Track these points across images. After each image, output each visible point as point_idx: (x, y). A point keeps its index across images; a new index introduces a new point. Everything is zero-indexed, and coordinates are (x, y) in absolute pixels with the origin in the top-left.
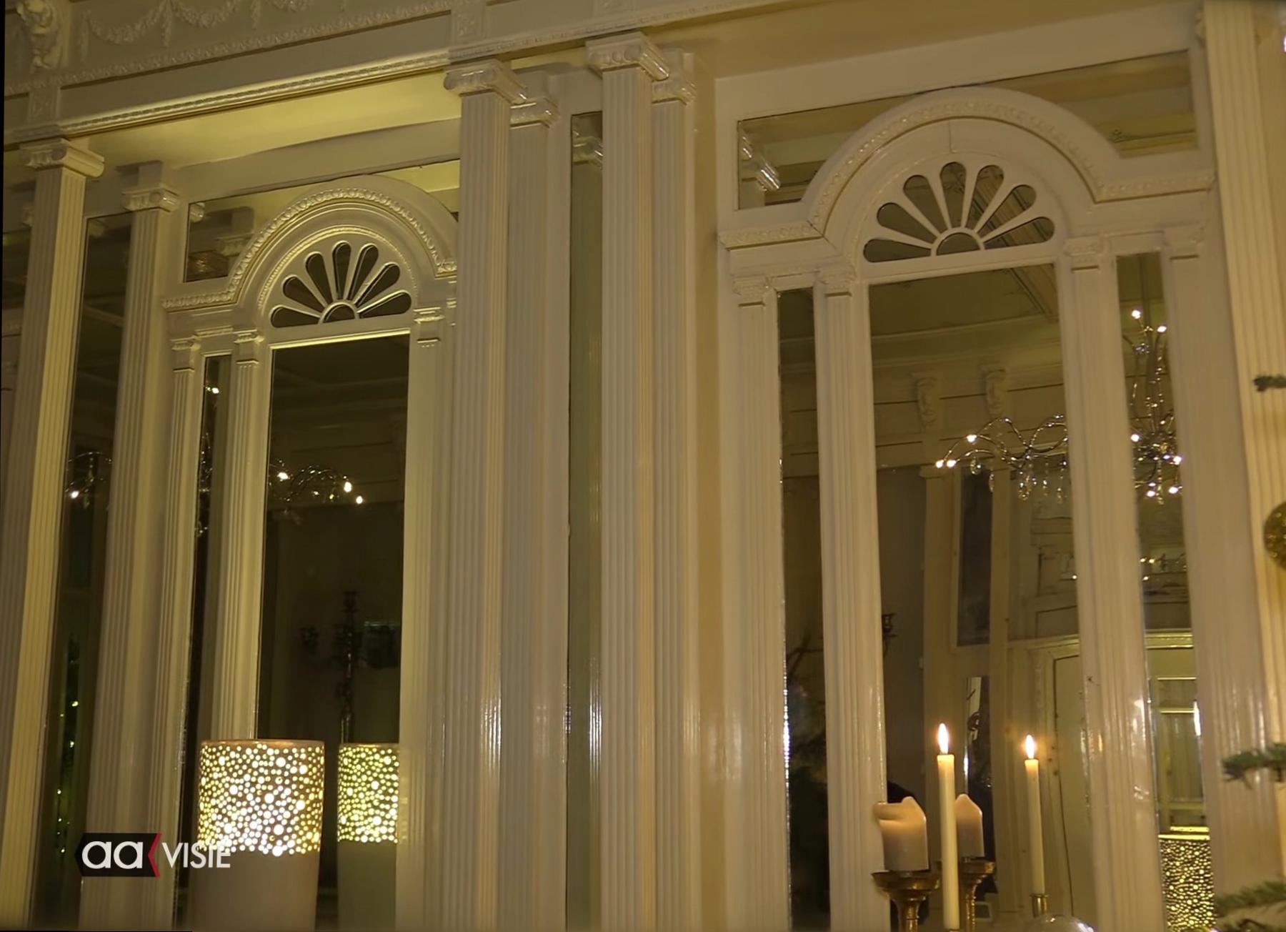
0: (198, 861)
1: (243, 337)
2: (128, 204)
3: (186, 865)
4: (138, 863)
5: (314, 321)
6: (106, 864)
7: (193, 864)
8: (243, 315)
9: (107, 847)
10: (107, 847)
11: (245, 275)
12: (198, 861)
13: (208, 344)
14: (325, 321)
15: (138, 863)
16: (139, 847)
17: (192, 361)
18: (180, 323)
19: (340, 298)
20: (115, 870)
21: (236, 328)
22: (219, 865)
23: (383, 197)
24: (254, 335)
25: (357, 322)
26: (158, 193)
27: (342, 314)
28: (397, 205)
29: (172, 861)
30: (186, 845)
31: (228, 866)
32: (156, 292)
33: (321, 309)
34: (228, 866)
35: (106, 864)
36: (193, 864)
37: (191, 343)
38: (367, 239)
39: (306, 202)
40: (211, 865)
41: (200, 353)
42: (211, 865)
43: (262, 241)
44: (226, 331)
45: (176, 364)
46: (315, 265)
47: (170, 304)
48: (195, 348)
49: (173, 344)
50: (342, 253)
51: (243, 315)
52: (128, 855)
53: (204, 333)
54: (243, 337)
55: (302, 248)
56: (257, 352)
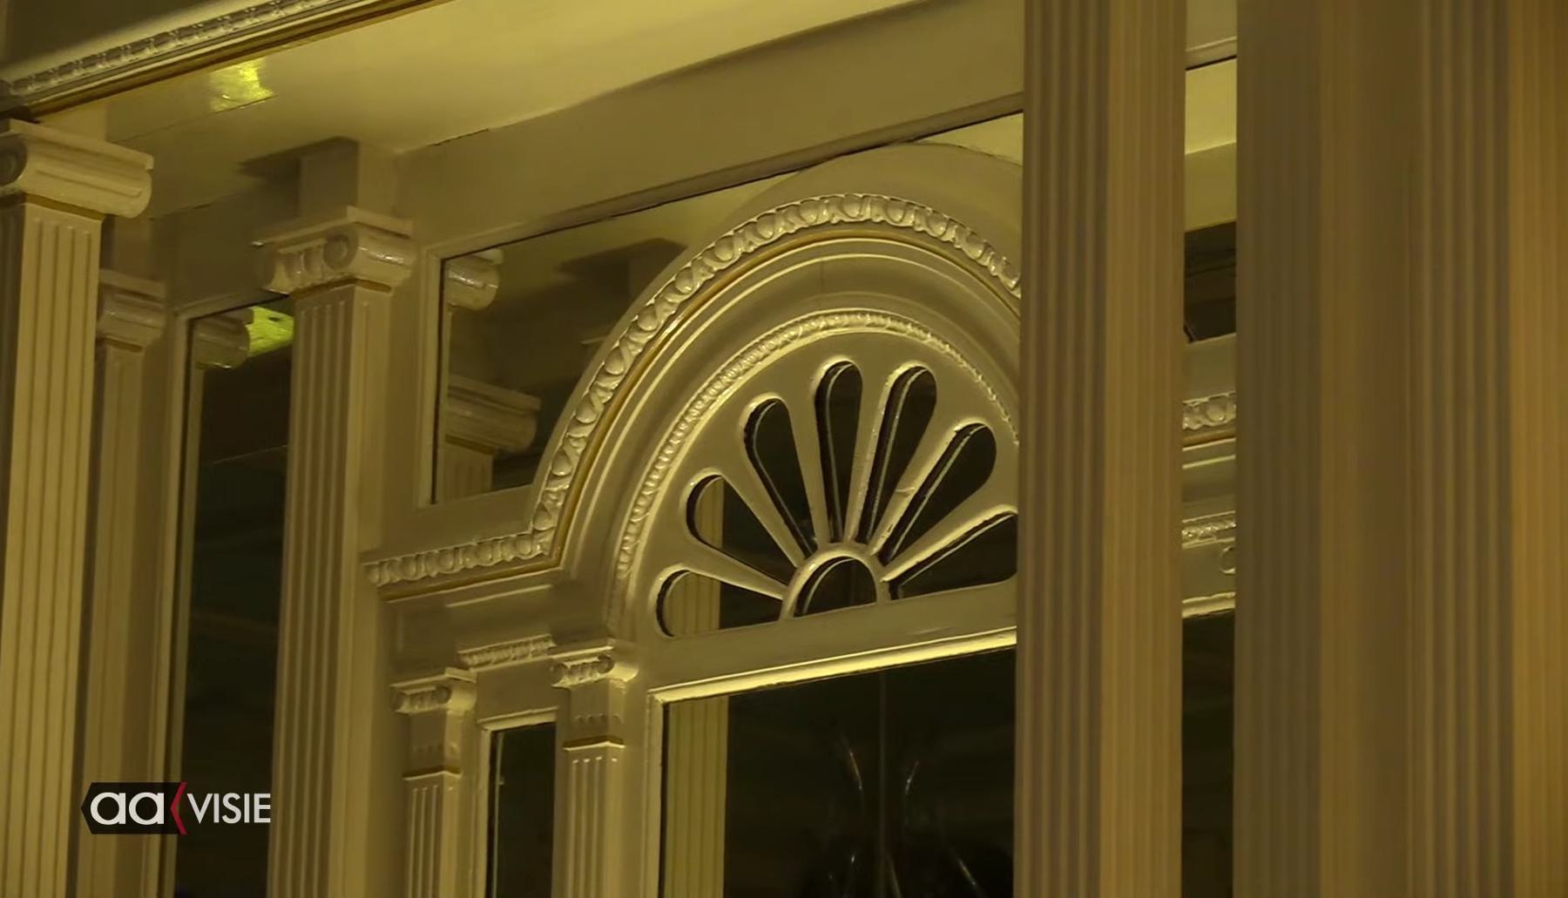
0: (232, 815)
1: (580, 667)
2: (269, 277)
3: (216, 820)
4: (159, 818)
5: (766, 610)
6: (120, 819)
7: (225, 818)
8: (578, 602)
9: (120, 798)
10: (120, 798)
11: (578, 479)
12: (232, 801)
13: (498, 691)
14: (799, 609)
15: (159, 818)
16: (159, 799)
17: (453, 745)
18: (424, 634)
19: (836, 538)
20: (130, 825)
21: (566, 638)
22: (257, 820)
23: (936, 217)
24: (605, 662)
25: (882, 611)
26: (340, 240)
27: (845, 587)
28: (973, 238)
29: (200, 815)
30: (217, 796)
31: (268, 820)
32: (354, 538)
33: (785, 574)
34: (268, 820)
35: (120, 819)
36: (225, 818)
37: (444, 691)
38: (907, 349)
39: (729, 242)
40: (247, 820)
41: (472, 725)
42: (247, 820)
43: (618, 369)
44: (532, 650)
45: (412, 753)
46: (767, 436)
47: (387, 576)
48: (459, 705)
49: (399, 696)
50: (839, 400)
51: (578, 602)
52: (147, 809)
53: (486, 659)
54: (580, 667)
55: (721, 393)
56: (617, 711)
